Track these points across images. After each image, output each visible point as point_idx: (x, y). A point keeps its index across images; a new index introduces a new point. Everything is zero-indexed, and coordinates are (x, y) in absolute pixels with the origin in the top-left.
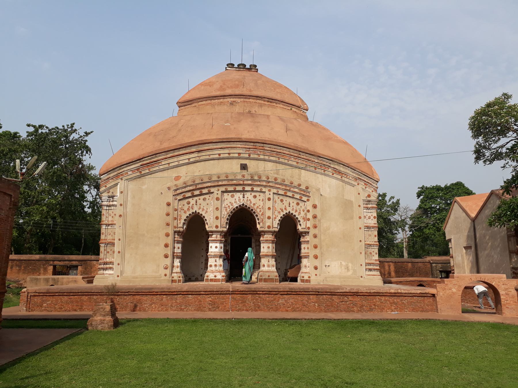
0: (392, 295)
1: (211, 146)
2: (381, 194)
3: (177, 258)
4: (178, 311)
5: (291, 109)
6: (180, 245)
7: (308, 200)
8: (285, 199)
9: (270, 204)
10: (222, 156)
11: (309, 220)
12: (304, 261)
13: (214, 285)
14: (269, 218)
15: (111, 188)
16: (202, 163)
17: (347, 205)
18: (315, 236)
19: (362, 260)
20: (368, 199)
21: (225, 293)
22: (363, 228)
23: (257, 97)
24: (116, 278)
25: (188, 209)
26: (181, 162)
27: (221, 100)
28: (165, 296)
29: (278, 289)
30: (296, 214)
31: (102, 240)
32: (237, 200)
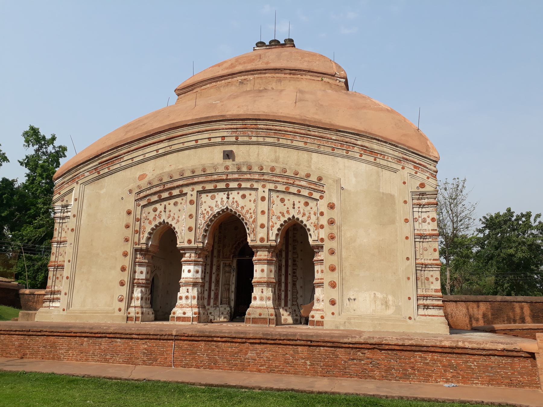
0: (445, 350)
1: (186, 131)
2: (524, 213)
3: (138, 286)
4: (101, 361)
5: (322, 80)
6: (144, 269)
7: (322, 197)
8: (286, 197)
9: (263, 206)
10: (200, 142)
11: (322, 227)
12: (318, 293)
13: (184, 325)
14: (262, 226)
15: (65, 194)
16: (175, 154)
17: (385, 201)
18: (332, 252)
19: (410, 289)
20: (421, 190)
21: (166, 337)
22: (412, 238)
23: (276, 70)
24: (62, 312)
25: (155, 218)
26: (147, 156)
27: (230, 80)
28: (86, 339)
29: (246, 333)
30: (304, 219)
31: (52, 262)
32: (219, 203)
